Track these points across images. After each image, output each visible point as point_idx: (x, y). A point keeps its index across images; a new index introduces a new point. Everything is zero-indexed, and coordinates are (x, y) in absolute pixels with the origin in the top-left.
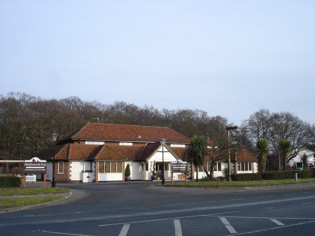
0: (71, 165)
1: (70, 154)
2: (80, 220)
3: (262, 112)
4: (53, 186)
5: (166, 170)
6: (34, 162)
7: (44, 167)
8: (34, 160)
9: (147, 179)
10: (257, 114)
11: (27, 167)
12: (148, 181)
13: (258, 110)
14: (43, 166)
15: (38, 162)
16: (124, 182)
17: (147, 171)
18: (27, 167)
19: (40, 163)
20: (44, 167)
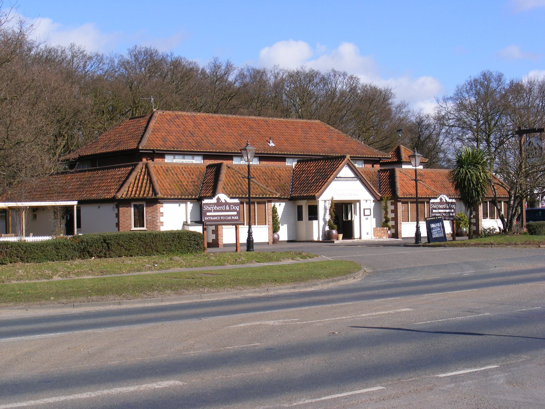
0: (162, 210)
1: (157, 188)
2: (381, 313)
3: (486, 77)
4: (248, 250)
5: (311, 219)
6: (219, 203)
7: (235, 213)
8: (441, 199)
9: (315, 238)
10: (474, 84)
11: (208, 214)
12: (318, 242)
13: (476, 73)
14: (234, 211)
15: (226, 203)
16: (272, 247)
17: (315, 222)
18: (208, 214)
19: (229, 204)
20: (235, 213)
